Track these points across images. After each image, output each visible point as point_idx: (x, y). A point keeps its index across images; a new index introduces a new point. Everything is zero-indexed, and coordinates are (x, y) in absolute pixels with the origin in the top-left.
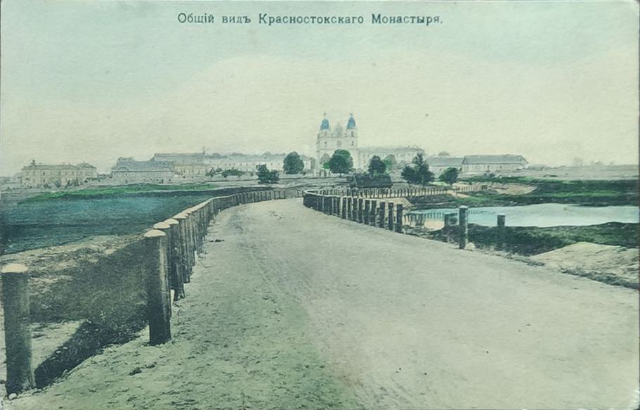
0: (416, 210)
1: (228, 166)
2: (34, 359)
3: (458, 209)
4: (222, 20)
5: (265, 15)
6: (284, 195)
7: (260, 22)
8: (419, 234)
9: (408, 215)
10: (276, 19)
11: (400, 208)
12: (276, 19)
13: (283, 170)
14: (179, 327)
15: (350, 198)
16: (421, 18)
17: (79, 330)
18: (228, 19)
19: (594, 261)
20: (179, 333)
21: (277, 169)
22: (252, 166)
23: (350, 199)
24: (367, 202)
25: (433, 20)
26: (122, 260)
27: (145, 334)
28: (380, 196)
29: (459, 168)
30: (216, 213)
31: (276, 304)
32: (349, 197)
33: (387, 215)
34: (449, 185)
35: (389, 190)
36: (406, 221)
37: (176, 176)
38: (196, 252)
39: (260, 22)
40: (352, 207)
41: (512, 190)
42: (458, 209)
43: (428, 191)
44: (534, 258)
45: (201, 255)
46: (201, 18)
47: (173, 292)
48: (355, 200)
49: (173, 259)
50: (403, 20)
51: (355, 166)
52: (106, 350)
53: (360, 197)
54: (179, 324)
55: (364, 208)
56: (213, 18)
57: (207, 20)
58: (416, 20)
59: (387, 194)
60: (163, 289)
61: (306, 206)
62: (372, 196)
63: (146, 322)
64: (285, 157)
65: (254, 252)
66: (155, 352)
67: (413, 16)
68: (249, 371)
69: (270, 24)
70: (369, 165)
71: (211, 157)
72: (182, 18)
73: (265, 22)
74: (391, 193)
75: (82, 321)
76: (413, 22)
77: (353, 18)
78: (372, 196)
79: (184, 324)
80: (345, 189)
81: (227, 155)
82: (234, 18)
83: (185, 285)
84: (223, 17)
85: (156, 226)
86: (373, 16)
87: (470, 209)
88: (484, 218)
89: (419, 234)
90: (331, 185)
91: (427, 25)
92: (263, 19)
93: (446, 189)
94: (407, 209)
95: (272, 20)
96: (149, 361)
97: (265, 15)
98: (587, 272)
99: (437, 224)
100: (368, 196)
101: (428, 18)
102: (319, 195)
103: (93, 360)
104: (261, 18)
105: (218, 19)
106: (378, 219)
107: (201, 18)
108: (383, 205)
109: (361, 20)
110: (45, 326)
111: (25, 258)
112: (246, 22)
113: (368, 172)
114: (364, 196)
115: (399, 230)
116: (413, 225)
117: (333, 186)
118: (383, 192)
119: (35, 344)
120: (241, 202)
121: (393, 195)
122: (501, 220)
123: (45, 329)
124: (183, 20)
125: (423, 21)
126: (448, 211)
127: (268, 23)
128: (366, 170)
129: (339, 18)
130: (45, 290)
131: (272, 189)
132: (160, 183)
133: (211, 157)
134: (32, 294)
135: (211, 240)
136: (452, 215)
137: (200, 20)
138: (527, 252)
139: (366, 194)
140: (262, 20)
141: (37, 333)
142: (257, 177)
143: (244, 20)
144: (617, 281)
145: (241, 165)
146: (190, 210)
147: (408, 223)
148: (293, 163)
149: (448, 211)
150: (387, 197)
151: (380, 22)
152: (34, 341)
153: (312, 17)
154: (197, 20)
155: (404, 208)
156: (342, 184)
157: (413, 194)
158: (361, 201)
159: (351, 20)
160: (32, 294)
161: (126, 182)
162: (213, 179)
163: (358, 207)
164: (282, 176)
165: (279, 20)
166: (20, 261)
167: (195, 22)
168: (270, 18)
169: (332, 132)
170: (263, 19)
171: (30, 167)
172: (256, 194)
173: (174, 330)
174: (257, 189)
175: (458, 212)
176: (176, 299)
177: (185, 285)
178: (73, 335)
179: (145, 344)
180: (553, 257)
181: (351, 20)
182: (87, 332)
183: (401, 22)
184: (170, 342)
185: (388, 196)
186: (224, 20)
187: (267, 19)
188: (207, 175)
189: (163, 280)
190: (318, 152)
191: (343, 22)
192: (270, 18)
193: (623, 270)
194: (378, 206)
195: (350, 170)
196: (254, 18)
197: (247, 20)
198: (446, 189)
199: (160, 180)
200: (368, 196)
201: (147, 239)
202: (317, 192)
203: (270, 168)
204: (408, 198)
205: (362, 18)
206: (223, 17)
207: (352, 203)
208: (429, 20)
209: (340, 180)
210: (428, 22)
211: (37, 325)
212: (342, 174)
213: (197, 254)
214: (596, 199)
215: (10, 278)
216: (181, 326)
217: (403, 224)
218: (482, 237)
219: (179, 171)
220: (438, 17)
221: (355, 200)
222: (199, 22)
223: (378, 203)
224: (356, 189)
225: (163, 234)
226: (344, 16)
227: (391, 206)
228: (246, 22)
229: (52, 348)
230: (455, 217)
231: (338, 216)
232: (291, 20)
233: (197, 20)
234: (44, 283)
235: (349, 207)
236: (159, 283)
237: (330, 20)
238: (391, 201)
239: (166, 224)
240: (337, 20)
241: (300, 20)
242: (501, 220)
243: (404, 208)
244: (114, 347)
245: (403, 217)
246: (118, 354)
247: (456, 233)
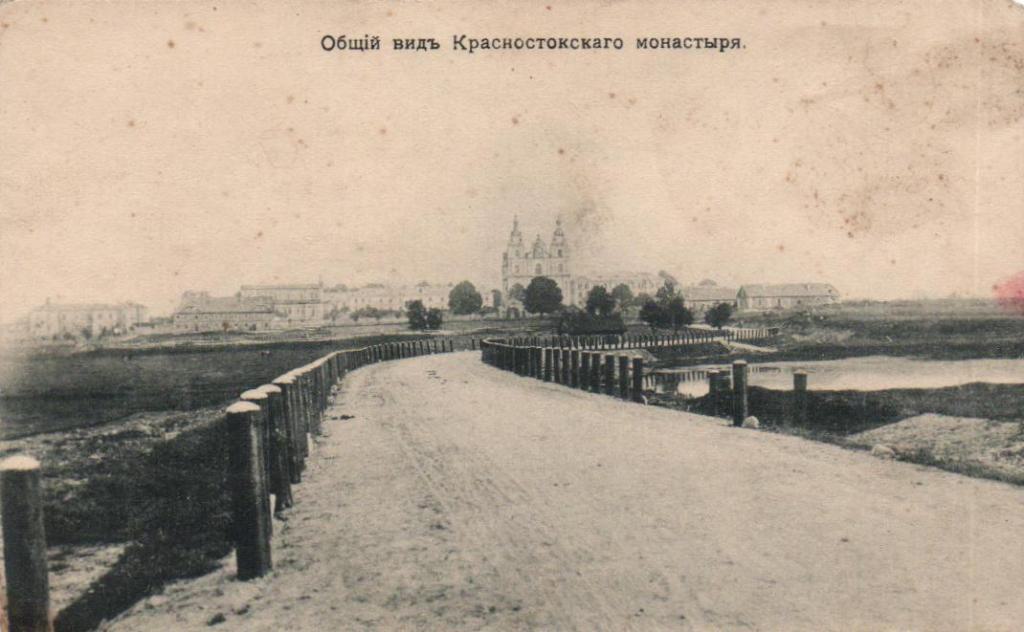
0: (664, 367)
1: (359, 301)
2: (52, 604)
3: (731, 366)
4: (393, 46)
5: (464, 37)
6: (449, 346)
7: (455, 48)
8: (668, 404)
9: (651, 374)
10: (480, 43)
11: (637, 362)
12: (480, 43)
13: (448, 308)
14: (285, 551)
15: (558, 351)
16: (711, 40)
17: (123, 559)
18: (404, 44)
19: (949, 443)
20: (284, 561)
21: (440, 308)
22: (399, 304)
23: (557, 352)
24: (585, 357)
25: (731, 45)
26: (191, 445)
27: (231, 563)
28: (606, 347)
29: (732, 304)
30: (341, 374)
31: (440, 516)
32: (556, 348)
33: (617, 374)
34: (716, 329)
35: (620, 338)
36: (647, 385)
37: (277, 319)
38: (309, 435)
39: (455, 48)
40: (561, 364)
41: (816, 336)
42: (731, 366)
43: (683, 339)
44: (855, 438)
45: (319, 439)
46: (358, 43)
47: (273, 498)
48: (565, 353)
49: (272, 448)
50: (682, 44)
51: (566, 301)
52: (168, 588)
53: (574, 349)
54: (285, 546)
55: (570, 367)
56: (378, 42)
57: (369, 46)
58: (702, 44)
59: (616, 343)
60: (257, 490)
61: (492, 364)
62: (593, 347)
63: (231, 544)
64: (451, 289)
65: (404, 434)
66: (243, 593)
67: (698, 37)
68: (398, 616)
69: (471, 51)
70: (587, 299)
71: (334, 291)
72: (328, 43)
73: (464, 48)
74: (624, 342)
75: (130, 544)
76: (698, 47)
77: (606, 40)
78: (593, 347)
79: (292, 546)
80: (548, 336)
81: (358, 287)
82: (413, 41)
83: (294, 488)
84: (395, 41)
85: (245, 395)
86: (639, 40)
87: (750, 366)
88: (778, 380)
89: (668, 404)
90: (527, 329)
91: (722, 51)
92: (460, 42)
93: (712, 334)
94: (650, 366)
95: (725, 43)
96: (238, 605)
97: (464, 37)
98: (938, 458)
99: (697, 388)
100: (587, 347)
101: (722, 40)
102: (507, 345)
103: (148, 602)
104: (456, 42)
105: (386, 45)
106: (603, 381)
107: (358, 43)
108: (610, 359)
109: (618, 44)
110: (70, 553)
111: (35, 446)
112: (432, 48)
113: (585, 311)
114: (580, 348)
115: (639, 400)
116: (659, 390)
117: (529, 333)
118: (610, 342)
119: (53, 579)
120: (380, 358)
121: (626, 345)
122: (800, 379)
123: (68, 557)
124: (325, 43)
125: (714, 46)
126: (714, 369)
127: (469, 49)
128: (582, 307)
129: (583, 40)
130: (69, 496)
131: (432, 337)
132: (251, 329)
133: (334, 291)
134: (48, 503)
135: (334, 416)
136: (723, 373)
137: (358, 45)
138: (842, 430)
139: (583, 345)
140: (458, 45)
141: (56, 563)
142: (406, 320)
143: (428, 45)
144: (987, 472)
145: (381, 301)
146: (298, 371)
147: (651, 387)
148: (465, 300)
149: (714, 369)
150: (616, 349)
151: (646, 47)
152: (51, 574)
153: (538, 39)
154: (353, 45)
155: (645, 365)
156: (543, 328)
157: (660, 343)
158: (575, 354)
159: (603, 43)
160: (48, 503)
161: (197, 329)
162: (337, 322)
163: (570, 363)
164: (447, 317)
165: (486, 45)
166: (27, 452)
167: (351, 48)
168: (471, 41)
169: (528, 251)
170: (460, 42)
171: (42, 307)
172: (406, 345)
173: (276, 557)
174: (408, 338)
175: (731, 370)
176: (278, 508)
177: (294, 488)
178: (114, 565)
179: (232, 579)
180: (885, 435)
181: (603, 43)
182: (136, 560)
183: (679, 46)
184: (270, 574)
185: (619, 346)
186: (396, 44)
187: (466, 43)
188: (326, 317)
189: (258, 477)
190: (505, 280)
191: (589, 47)
192: (471, 41)
193: (994, 454)
194: (603, 362)
195: (557, 308)
196: (446, 42)
197: (435, 46)
198: (712, 334)
199: (250, 324)
200: (587, 347)
201: (231, 416)
202: (503, 341)
203: (428, 305)
204: (650, 350)
205: (616, 47)
206: (395, 41)
207: (561, 357)
208: (725, 43)
209: (543, 322)
210: (722, 47)
211: (56, 551)
212: (545, 314)
213: (312, 437)
214: (961, 348)
215: (16, 478)
216: (289, 550)
217: (644, 387)
218: (772, 411)
219: (281, 311)
220: (738, 40)
221: (565, 353)
222: (356, 48)
223: (603, 357)
224: (567, 335)
225: (255, 407)
226: (591, 36)
227: (624, 361)
228: (432, 48)
229: (80, 586)
230: (725, 377)
231: (539, 378)
232: (505, 44)
233: (358, 45)
234: (66, 486)
235: (556, 362)
236: (250, 485)
237: (568, 43)
238: (623, 354)
239: (261, 392)
240: (580, 43)
241: (519, 44)
242: (800, 379)
243: (645, 365)
244: (181, 584)
245: (644, 380)
246: (189, 593)
247: (730, 402)
